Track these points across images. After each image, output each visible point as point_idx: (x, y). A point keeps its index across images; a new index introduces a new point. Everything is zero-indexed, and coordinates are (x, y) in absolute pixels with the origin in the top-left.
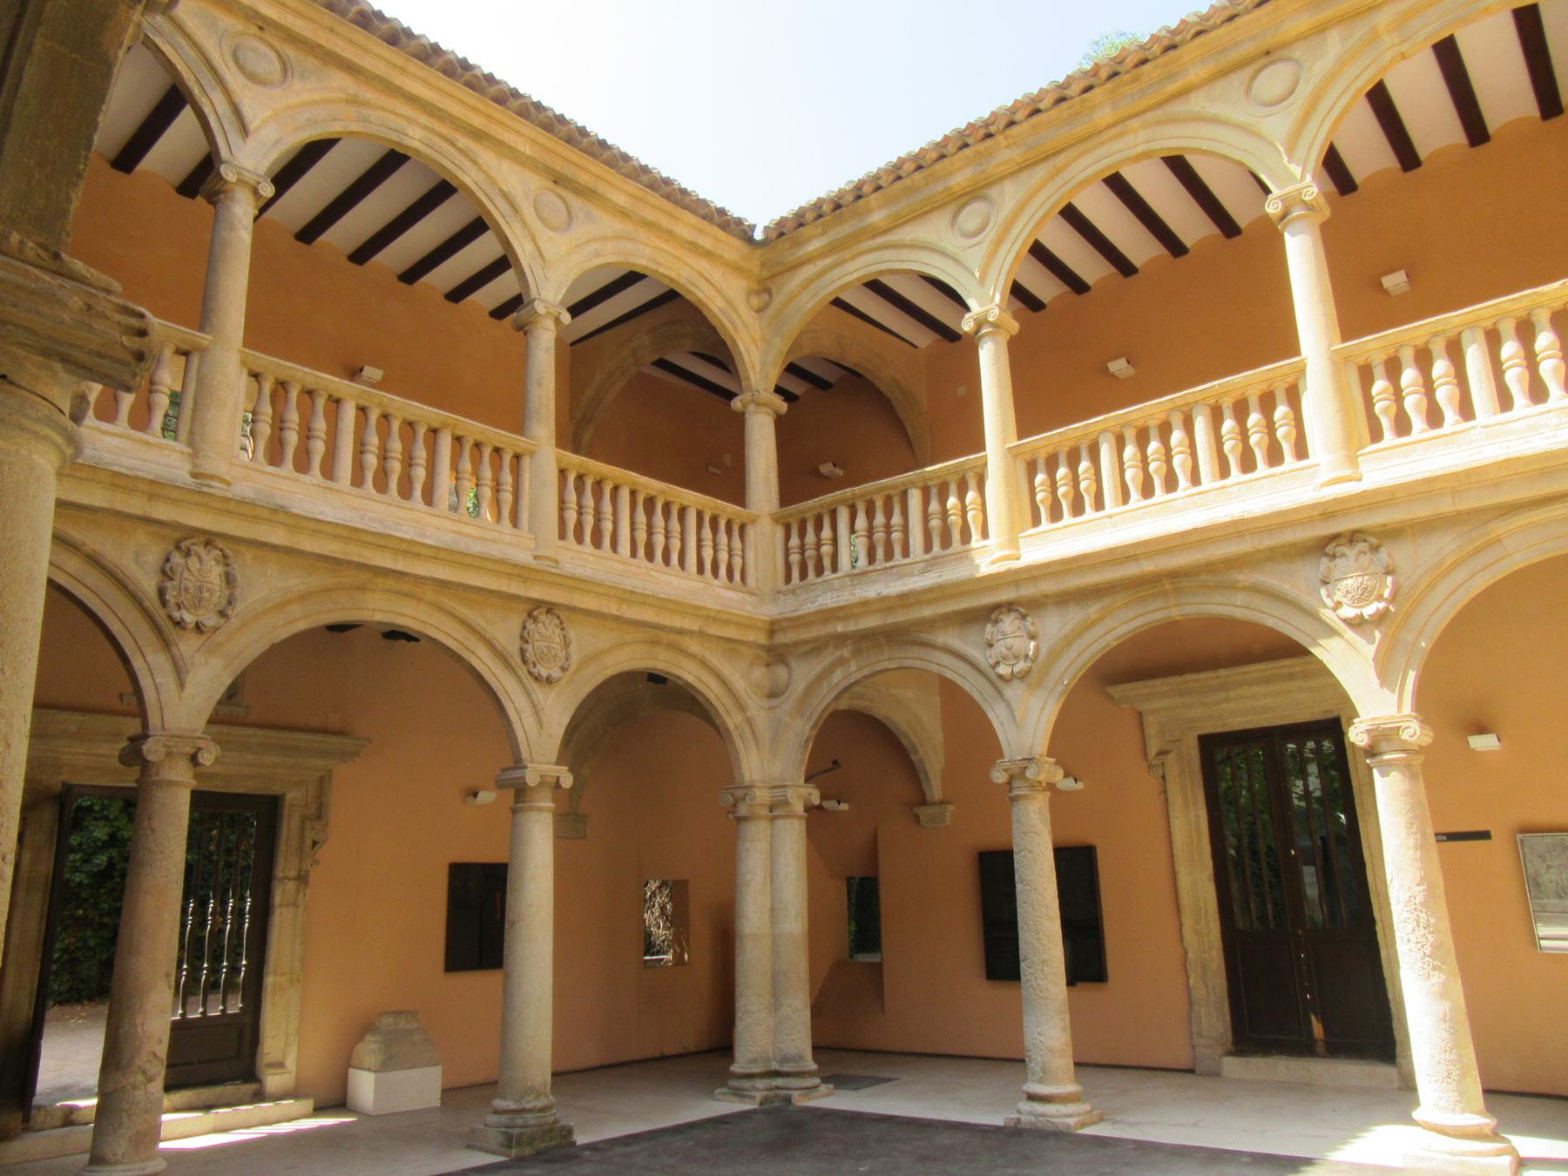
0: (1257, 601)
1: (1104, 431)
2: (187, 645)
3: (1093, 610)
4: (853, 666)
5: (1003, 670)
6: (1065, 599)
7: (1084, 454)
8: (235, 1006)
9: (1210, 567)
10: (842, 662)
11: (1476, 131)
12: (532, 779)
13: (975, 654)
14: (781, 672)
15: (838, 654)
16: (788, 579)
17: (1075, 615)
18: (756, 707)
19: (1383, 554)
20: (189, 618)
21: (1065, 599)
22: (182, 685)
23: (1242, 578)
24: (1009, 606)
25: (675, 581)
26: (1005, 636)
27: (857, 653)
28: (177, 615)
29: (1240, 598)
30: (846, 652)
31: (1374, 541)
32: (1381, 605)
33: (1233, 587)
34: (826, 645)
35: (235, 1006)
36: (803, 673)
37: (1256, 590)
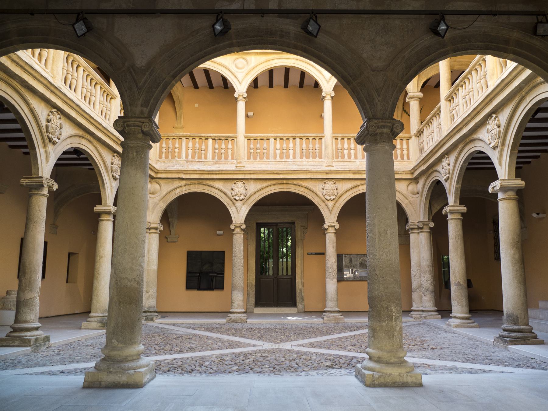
5: (237, 198)
13: (229, 193)
16: (160, 157)
17: (259, 185)
18: (411, 198)
25: (341, 164)
36: (421, 182)
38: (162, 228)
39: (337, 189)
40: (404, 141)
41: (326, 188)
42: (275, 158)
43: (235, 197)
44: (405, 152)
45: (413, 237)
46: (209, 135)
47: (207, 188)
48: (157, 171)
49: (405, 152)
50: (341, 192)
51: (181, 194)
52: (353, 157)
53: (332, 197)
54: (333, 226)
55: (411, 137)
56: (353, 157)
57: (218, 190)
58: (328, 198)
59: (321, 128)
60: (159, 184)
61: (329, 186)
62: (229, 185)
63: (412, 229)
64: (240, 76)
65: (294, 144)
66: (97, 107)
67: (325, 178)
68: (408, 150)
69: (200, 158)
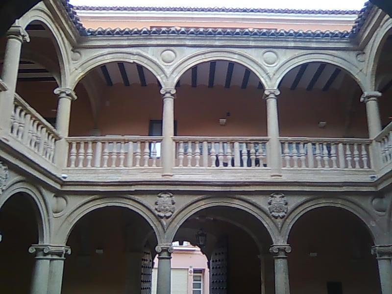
11: (310, 87)
13: (153, 208)
14: (62, 201)
19: (285, 198)
31: (172, 195)
32: (284, 214)
38: (69, 252)
39: (286, 204)
40: (90, 145)
41: (273, 203)
42: (242, 165)
43: (273, 213)
44: (365, 159)
45: (157, 267)
46: (308, 139)
47: (131, 202)
48: (63, 183)
49: (365, 159)
50: (290, 207)
52: (245, 163)
53: (281, 214)
54: (284, 250)
55: (371, 142)
56: (245, 163)
57: (144, 207)
58: (276, 214)
59: (264, 131)
60: (64, 198)
61: (277, 200)
62: (155, 198)
63: (382, 254)
64: (168, 71)
65: (201, 149)
66: (26, 137)
67: (267, 189)
68: (368, 155)
69: (85, 165)
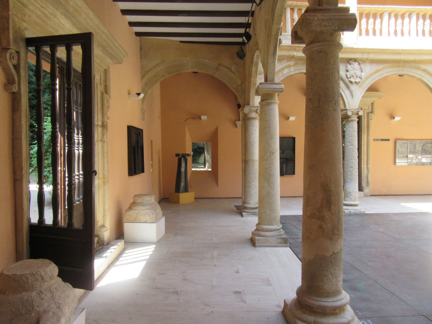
0: (423, 74)
1: (387, 11)
2: (353, 87)
3: (381, 66)
4: (292, 69)
5: (352, 80)
6: (373, 62)
7: (378, 16)
8: (207, 168)
9: (414, 62)
10: (289, 66)
12: (349, 113)
15: (289, 63)
17: (375, 67)
20: (353, 81)
21: (373, 62)
22: (352, 96)
23: (423, 66)
24: (355, 60)
26: (354, 69)
27: (295, 65)
28: (350, 79)
29: (419, 72)
30: (292, 63)
33: (418, 69)
34: (284, 59)
35: (207, 168)
37: (424, 71)
51: (289, 74)
